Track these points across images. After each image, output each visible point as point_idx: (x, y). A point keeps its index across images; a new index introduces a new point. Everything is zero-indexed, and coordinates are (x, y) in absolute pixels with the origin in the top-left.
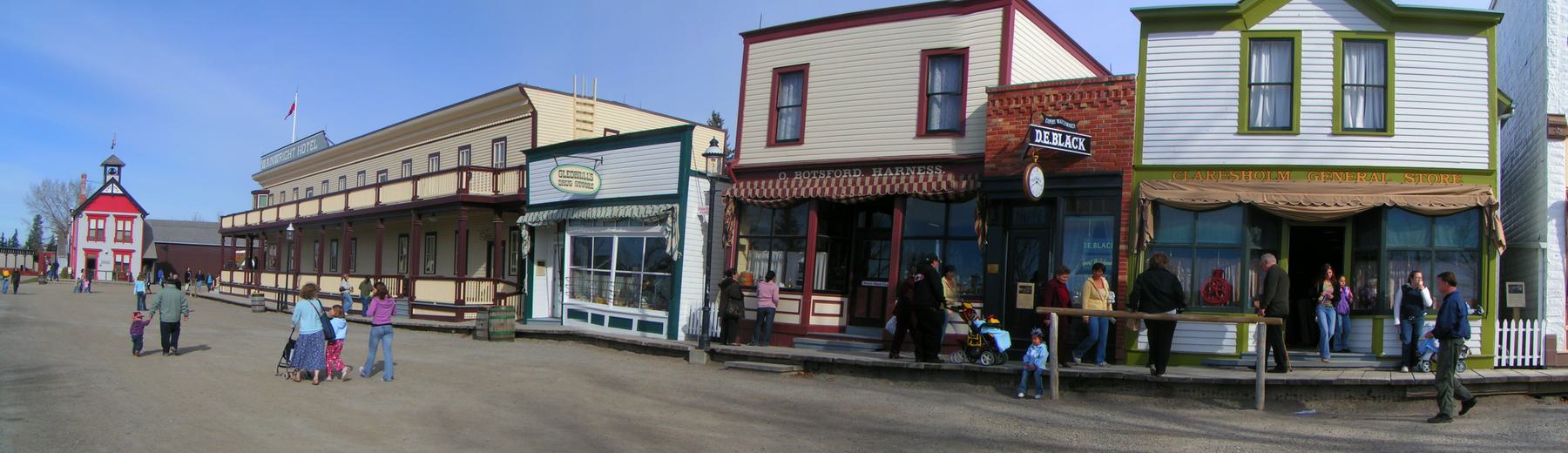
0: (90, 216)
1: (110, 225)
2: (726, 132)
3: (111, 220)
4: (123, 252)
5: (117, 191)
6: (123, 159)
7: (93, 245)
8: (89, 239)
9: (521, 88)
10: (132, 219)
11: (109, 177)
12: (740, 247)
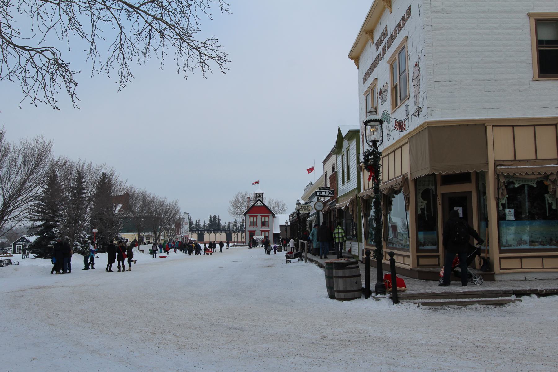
0: (250, 216)
3: (259, 217)
4: (265, 231)
5: (261, 204)
7: (252, 229)
8: (250, 226)
10: (268, 216)
11: (257, 199)
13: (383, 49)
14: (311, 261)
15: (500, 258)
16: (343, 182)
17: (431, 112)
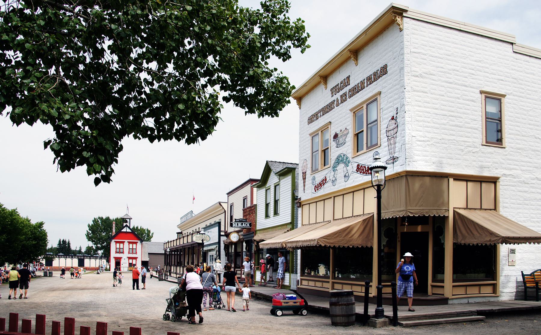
0: (116, 242)
1: (126, 246)
2: (293, 225)
3: (126, 244)
4: (133, 258)
5: (129, 230)
6: (131, 216)
8: (116, 252)
9: (220, 203)
10: (136, 243)
12: (268, 270)
13: (341, 96)
14: (528, 320)
15: (453, 286)
16: (267, 216)
17: (409, 163)
